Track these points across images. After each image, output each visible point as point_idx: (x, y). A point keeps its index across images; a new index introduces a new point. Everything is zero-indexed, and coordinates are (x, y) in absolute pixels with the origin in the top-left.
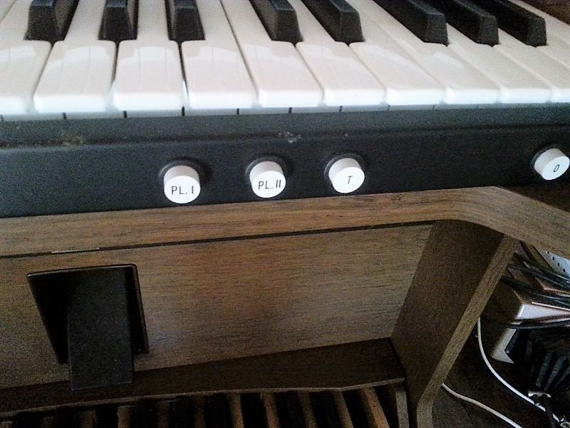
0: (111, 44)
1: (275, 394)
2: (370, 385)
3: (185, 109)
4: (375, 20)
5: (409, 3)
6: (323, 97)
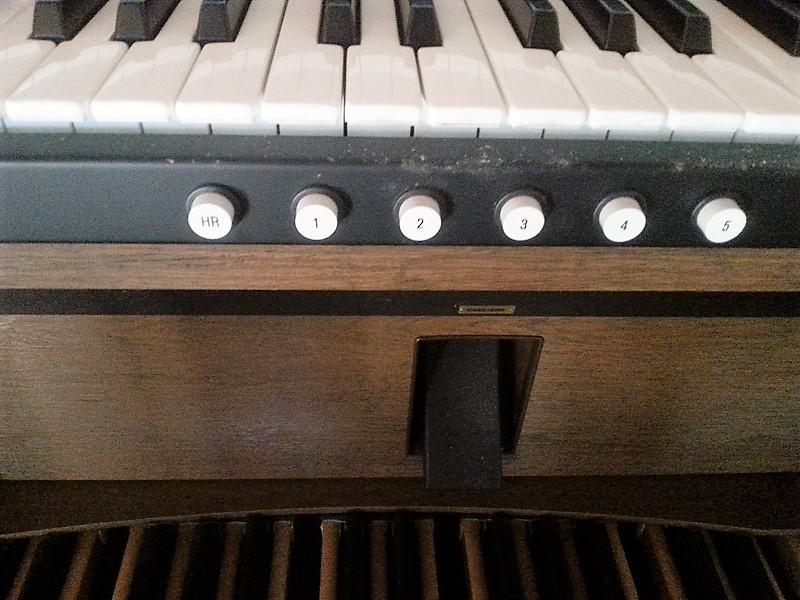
0: (339, 49)
1: (662, 526)
3: (546, 132)
4: (727, 27)
5: (669, 6)
6: (587, 119)
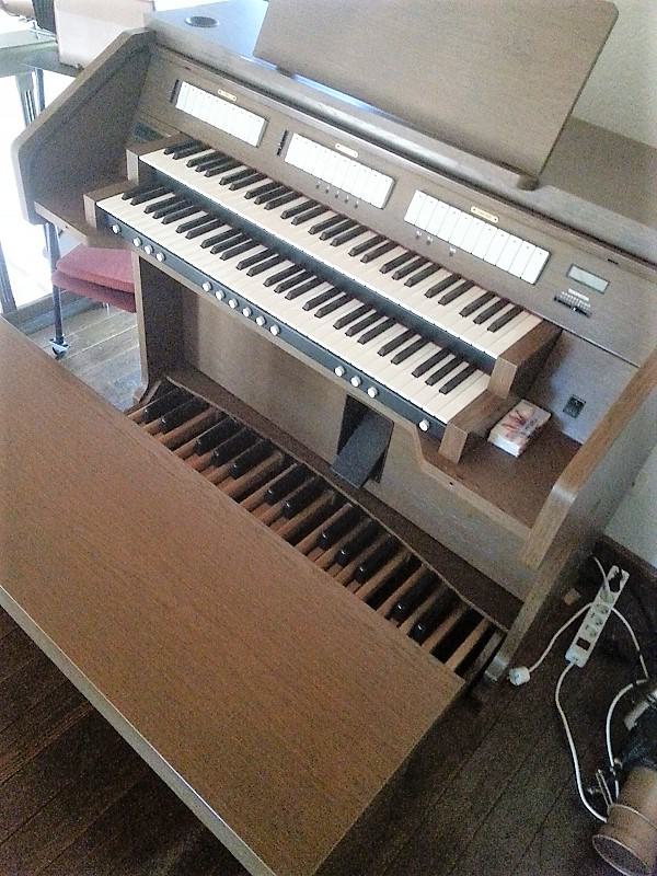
2: (492, 620)
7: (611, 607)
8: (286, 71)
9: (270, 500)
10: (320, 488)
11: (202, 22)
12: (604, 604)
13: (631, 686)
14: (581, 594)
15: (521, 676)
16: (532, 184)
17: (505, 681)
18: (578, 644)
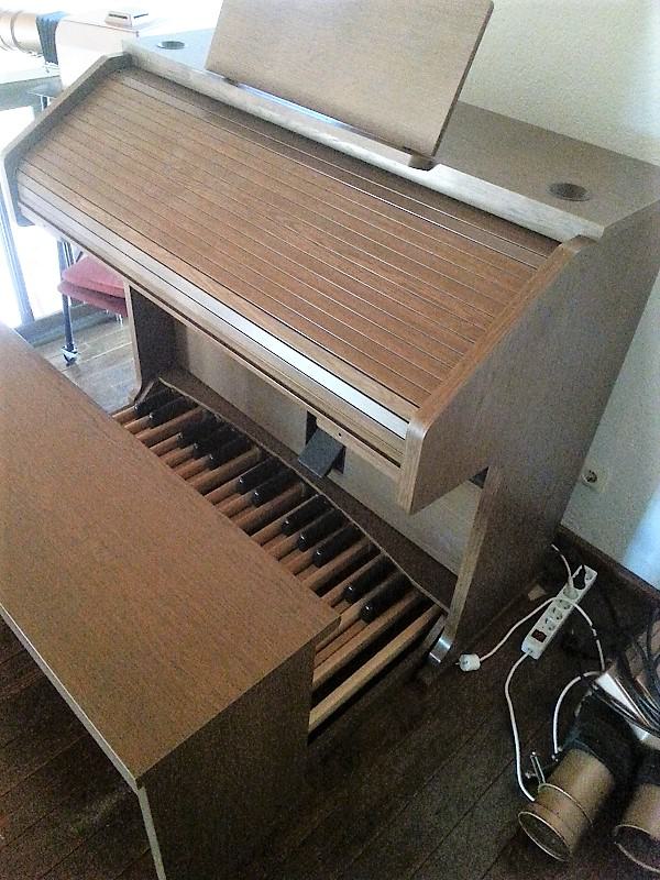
7: (574, 603)
8: (230, 81)
9: (286, 530)
10: (292, 479)
11: (171, 45)
12: (567, 599)
13: (579, 678)
14: (546, 591)
15: (471, 662)
16: (427, 165)
17: (452, 660)
18: (533, 635)
